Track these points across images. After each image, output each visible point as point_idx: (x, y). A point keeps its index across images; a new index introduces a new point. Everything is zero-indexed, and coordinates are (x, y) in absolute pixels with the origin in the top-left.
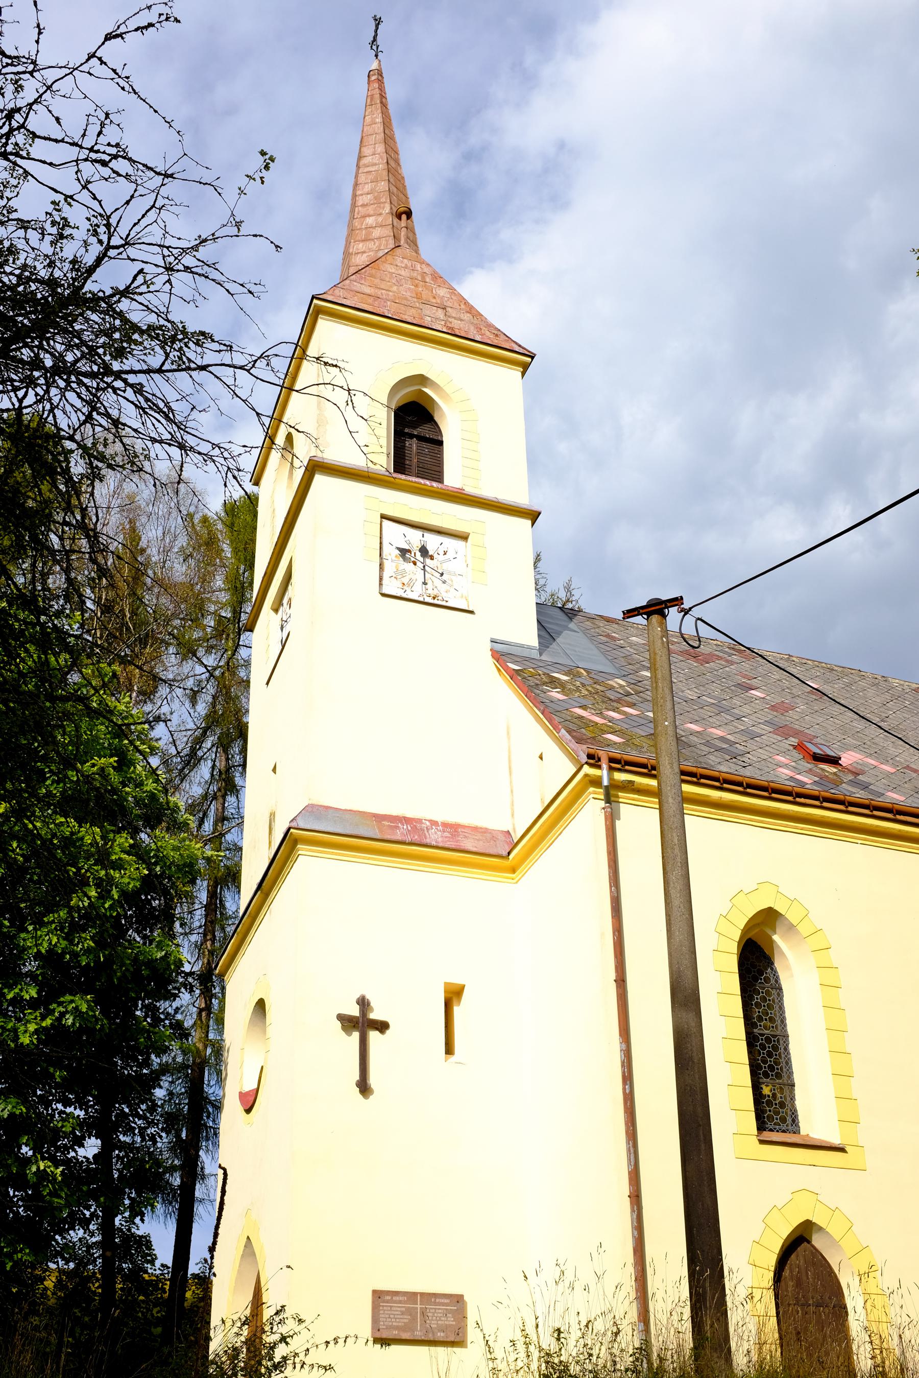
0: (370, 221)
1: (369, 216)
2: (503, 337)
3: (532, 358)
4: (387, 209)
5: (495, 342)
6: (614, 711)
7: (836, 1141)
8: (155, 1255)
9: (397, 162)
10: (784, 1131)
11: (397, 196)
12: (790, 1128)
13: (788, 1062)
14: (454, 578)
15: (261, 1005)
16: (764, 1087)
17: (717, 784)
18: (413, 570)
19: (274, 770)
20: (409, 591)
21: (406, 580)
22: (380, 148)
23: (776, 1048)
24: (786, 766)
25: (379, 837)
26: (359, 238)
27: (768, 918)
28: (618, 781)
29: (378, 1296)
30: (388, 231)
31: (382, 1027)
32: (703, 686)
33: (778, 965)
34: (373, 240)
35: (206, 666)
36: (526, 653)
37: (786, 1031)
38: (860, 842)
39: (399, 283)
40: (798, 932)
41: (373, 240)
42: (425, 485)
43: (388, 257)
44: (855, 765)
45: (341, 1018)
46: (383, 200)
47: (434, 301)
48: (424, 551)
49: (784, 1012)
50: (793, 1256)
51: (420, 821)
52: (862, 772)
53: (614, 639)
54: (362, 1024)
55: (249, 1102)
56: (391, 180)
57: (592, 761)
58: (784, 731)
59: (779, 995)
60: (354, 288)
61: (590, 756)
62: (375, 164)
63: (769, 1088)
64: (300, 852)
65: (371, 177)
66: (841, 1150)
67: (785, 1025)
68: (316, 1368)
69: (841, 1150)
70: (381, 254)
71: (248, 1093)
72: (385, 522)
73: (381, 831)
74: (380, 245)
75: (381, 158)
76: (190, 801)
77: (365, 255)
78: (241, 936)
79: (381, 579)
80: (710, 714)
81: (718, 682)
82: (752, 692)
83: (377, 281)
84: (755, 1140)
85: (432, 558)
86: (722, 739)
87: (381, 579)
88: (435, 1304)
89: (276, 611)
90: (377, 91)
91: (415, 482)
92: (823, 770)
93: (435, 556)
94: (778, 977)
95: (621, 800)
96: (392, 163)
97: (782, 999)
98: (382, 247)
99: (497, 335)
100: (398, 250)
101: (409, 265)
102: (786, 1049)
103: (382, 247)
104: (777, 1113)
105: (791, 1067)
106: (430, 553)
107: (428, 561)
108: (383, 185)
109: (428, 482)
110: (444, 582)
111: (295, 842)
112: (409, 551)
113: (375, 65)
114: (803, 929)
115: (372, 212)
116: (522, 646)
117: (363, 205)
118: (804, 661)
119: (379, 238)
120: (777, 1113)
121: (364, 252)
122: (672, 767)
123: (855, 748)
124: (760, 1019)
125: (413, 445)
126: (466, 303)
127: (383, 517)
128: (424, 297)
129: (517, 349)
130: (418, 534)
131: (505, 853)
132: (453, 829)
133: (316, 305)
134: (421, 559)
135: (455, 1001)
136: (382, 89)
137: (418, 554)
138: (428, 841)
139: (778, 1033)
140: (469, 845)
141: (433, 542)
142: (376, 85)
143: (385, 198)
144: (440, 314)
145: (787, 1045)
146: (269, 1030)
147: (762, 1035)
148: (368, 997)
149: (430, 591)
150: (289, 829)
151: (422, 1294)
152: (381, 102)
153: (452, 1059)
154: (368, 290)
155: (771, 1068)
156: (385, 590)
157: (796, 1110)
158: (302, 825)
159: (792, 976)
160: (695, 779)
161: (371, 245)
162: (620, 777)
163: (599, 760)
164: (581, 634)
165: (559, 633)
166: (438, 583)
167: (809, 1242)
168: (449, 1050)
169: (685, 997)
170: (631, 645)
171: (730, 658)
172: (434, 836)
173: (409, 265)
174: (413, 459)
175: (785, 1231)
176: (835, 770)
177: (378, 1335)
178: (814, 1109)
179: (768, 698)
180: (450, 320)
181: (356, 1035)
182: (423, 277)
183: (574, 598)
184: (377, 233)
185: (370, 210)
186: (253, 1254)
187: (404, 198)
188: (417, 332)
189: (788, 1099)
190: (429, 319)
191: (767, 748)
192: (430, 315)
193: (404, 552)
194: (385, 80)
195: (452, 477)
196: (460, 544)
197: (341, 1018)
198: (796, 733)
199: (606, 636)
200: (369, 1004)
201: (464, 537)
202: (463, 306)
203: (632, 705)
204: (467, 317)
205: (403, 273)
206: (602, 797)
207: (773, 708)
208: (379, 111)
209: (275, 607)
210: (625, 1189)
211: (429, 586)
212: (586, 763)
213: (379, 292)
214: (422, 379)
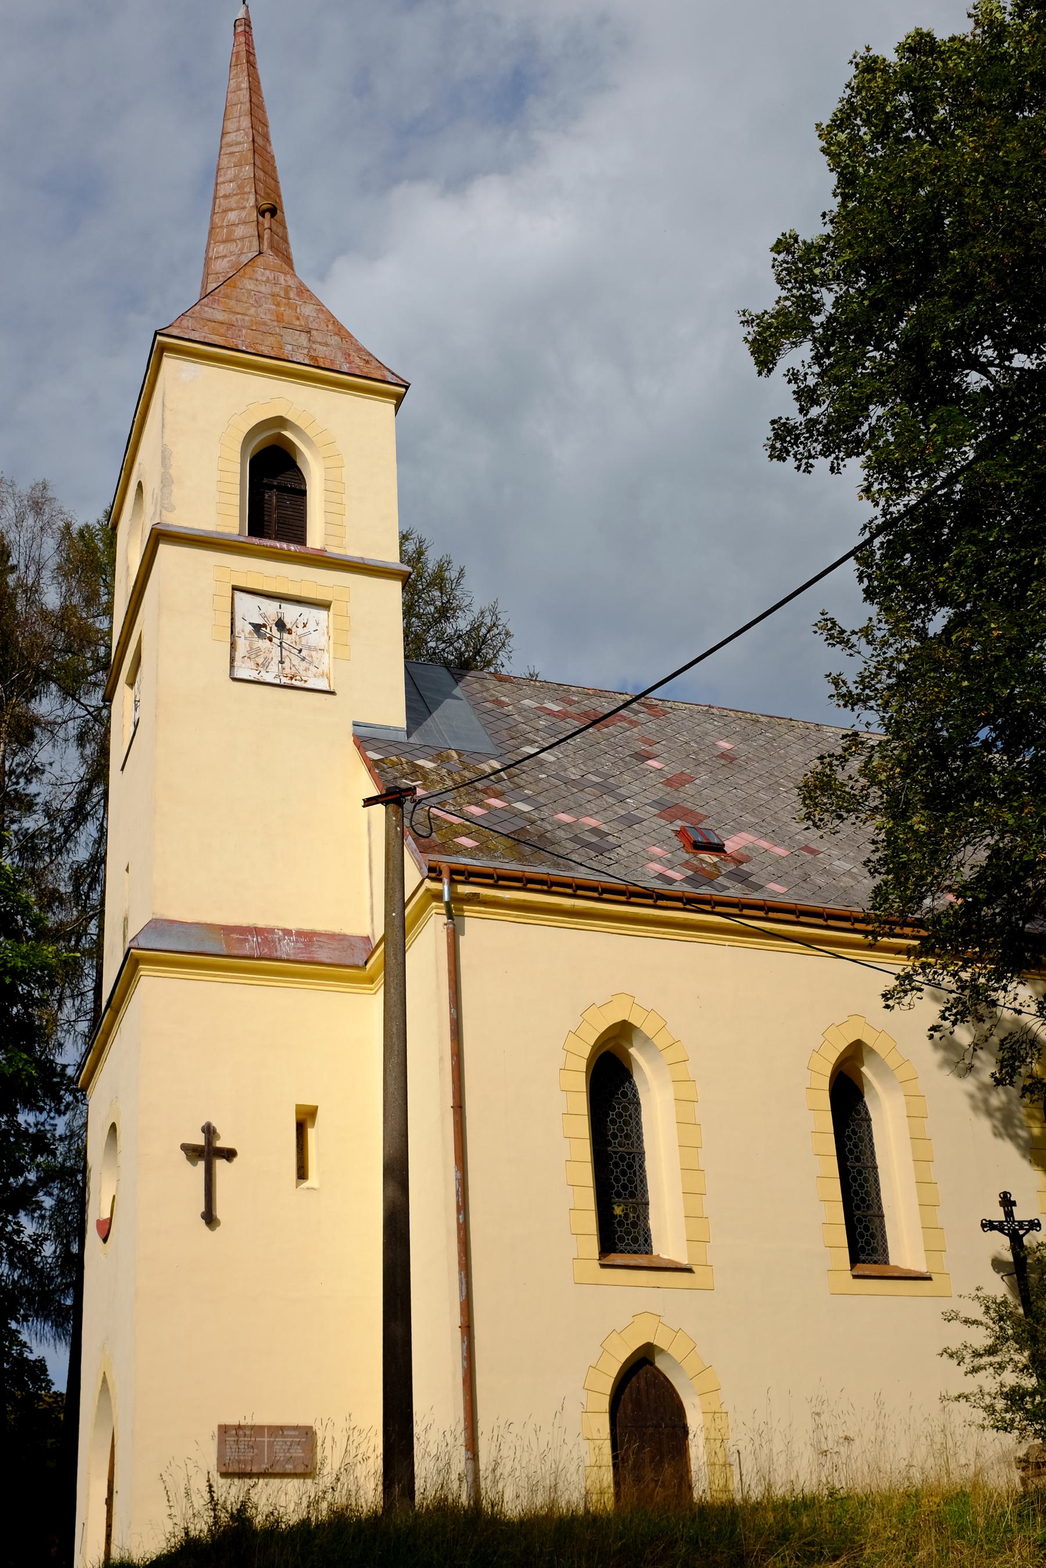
0: (232, 216)
1: (231, 210)
2: (374, 363)
3: (407, 388)
4: (252, 202)
5: (365, 371)
6: (477, 804)
7: (684, 1261)
8: (50, 1381)
9: (266, 138)
10: (635, 1252)
11: (265, 182)
12: (642, 1248)
13: (643, 1180)
14: (314, 653)
15: (113, 1127)
16: (616, 1207)
17: (570, 891)
18: (266, 651)
19: (127, 870)
20: (263, 673)
21: (260, 660)
22: (246, 122)
23: (630, 1166)
24: (658, 860)
25: (225, 953)
26: (219, 238)
27: (623, 1031)
28: (462, 894)
29: (224, 1429)
30: (252, 230)
31: (229, 1154)
32: (592, 760)
33: (636, 1078)
34: (235, 240)
35: (85, 706)
36: (392, 737)
37: (642, 1148)
38: (728, 943)
39: (258, 304)
40: (653, 1045)
41: (235, 240)
42: (282, 549)
43: (248, 269)
44: (742, 851)
45: (185, 1147)
46: (247, 189)
47: (297, 323)
48: (281, 625)
49: (641, 1128)
50: (634, 1379)
51: (271, 931)
52: (748, 859)
53: (502, 704)
54: (209, 1152)
55: (105, 1230)
56: (258, 163)
57: (433, 875)
58: (668, 811)
59: (636, 1110)
60: (205, 315)
61: (431, 869)
62: (239, 143)
63: (621, 1208)
64: (142, 973)
65: (234, 160)
66: (689, 1270)
67: (642, 1142)
68: (171, 1504)
69: (689, 1270)
70: (244, 259)
71: (105, 1220)
72: (238, 594)
73: (228, 945)
74: (243, 247)
75: (247, 134)
76: (75, 866)
77: (226, 260)
78: (97, 1052)
79: (232, 660)
80: (590, 798)
81: (612, 752)
82: (650, 762)
83: (232, 303)
84: (596, 1263)
85: (290, 632)
86: (595, 831)
87: (232, 660)
88: (283, 1436)
89: (131, 685)
90: (243, 47)
91: (271, 547)
92: (702, 860)
93: (294, 629)
94: (636, 1091)
95: (466, 914)
96: (259, 140)
97: (639, 1114)
98: (245, 251)
99: (367, 362)
100: (261, 259)
101: (271, 277)
102: (642, 1166)
103: (245, 251)
104: (629, 1233)
105: (645, 1185)
106: (288, 626)
107: (286, 635)
108: (248, 170)
109: (285, 546)
110: (303, 659)
111: (137, 962)
112: (265, 626)
113: (241, 14)
114: (660, 1042)
115: (234, 206)
116: (388, 728)
117: (225, 197)
118: (725, 713)
119: (242, 239)
120: (629, 1233)
121: (225, 256)
122: (396, 958)
123: (751, 827)
124: (615, 1136)
125: (272, 497)
126: (335, 322)
127: (235, 588)
128: (286, 318)
129: (390, 378)
130: (275, 604)
131: (361, 963)
132: (307, 937)
133: (160, 342)
134: (278, 635)
135: (309, 1124)
136: (249, 43)
137: (275, 628)
138: (278, 954)
139: (634, 1150)
140: (322, 955)
141: (291, 613)
142: (242, 39)
143: (249, 188)
144: (303, 339)
145: (643, 1162)
146: (120, 1157)
147: (616, 1153)
148: (214, 1124)
149: (287, 671)
150: (129, 949)
151: (269, 1427)
152: (248, 62)
153: (306, 1184)
154: (220, 316)
155: (625, 1187)
156: (239, 674)
157: (649, 1230)
158: (142, 945)
159: (649, 1090)
160: (545, 888)
161: (232, 247)
162: (463, 889)
163: (441, 872)
164: (464, 702)
165: (438, 704)
166: (296, 661)
167: (652, 1364)
168: (302, 1173)
169: (396, 1172)
170: (521, 711)
171: (634, 718)
172: (286, 948)
173: (271, 277)
174: (273, 516)
175: (623, 1354)
176: (716, 859)
177: (224, 1470)
178: (668, 1230)
179: (666, 769)
180: (314, 346)
181: (201, 1165)
182: (287, 292)
183: (500, 622)
184: (239, 231)
185: (233, 202)
186: (108, 1390)
187: (273, 182)
188: (275, 365)
189: (642, 1218)
190: (290, 347)
191: (645, 838)
192: (294, 344)
193: (257, 628)
194: (254, 32)
195: (316, 538)
196: (322, 614)
197: (185, 1147)
198: (686, 813)
199: (493, 702)
200: (215, 1131)
201: (325, 606)
202: (331, 327)
203: (498, 795)
204: (335, 340)
205: (263, 289)
206: (444, 912)
207: (668, 782)
208: (245, 73)
209: (130, 681)
210: (456, 1318)
211: (287, 665)
212: (428, 877)
213: (234, 318)
214: (280, 422)
